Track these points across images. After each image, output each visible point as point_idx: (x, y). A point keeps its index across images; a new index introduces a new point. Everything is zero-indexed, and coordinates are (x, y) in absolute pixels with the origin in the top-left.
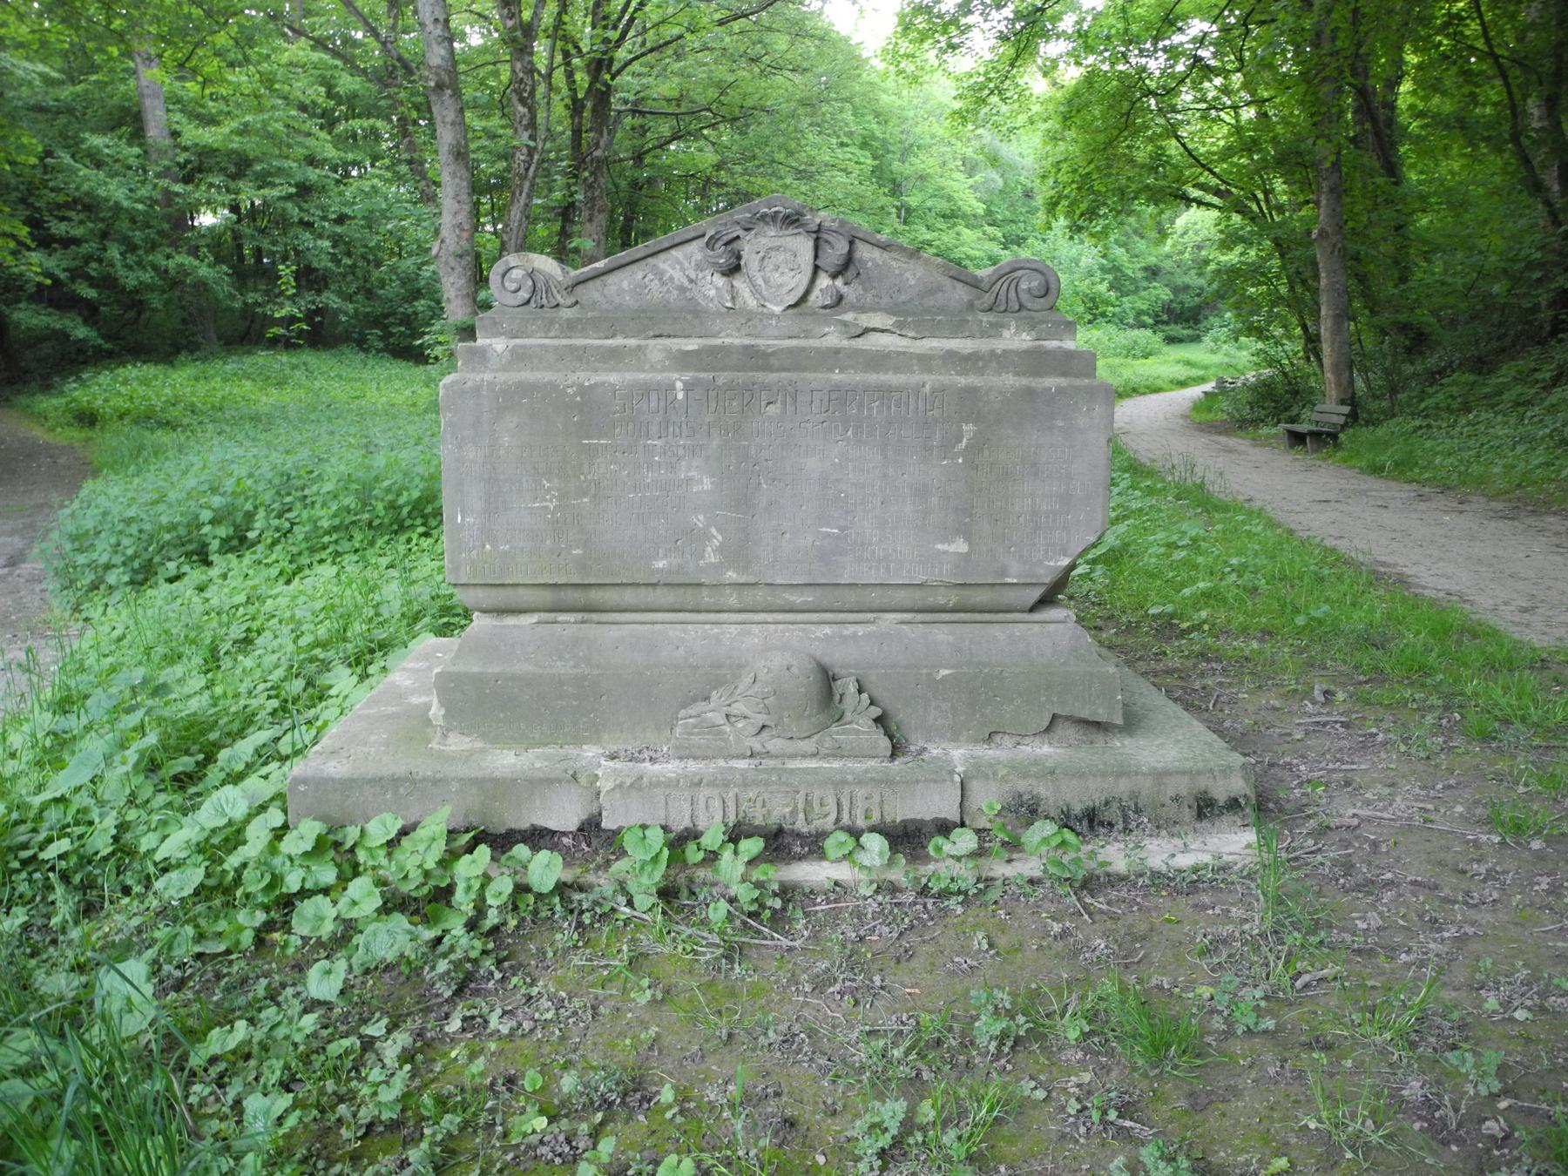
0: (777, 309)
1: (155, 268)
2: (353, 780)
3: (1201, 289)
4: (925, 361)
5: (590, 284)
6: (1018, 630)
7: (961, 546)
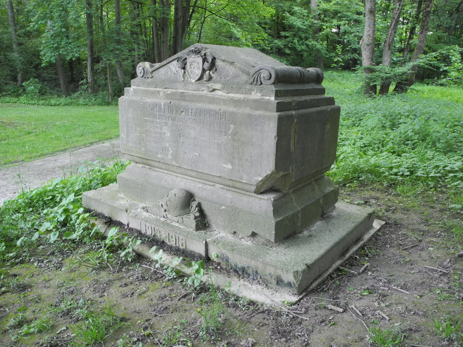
0: (193, 81)
1: (307, 45)
6: (251, 199)
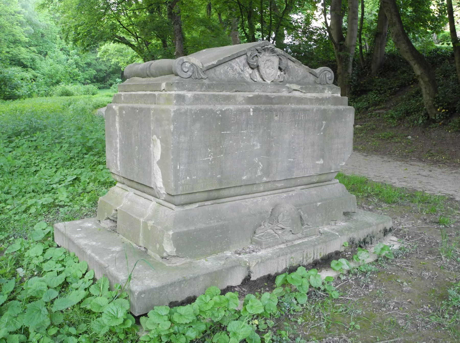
2: (163, 286)
3: (106, 70)
4: (311, 100)
5: (210, 70)
7: (321, 162)
